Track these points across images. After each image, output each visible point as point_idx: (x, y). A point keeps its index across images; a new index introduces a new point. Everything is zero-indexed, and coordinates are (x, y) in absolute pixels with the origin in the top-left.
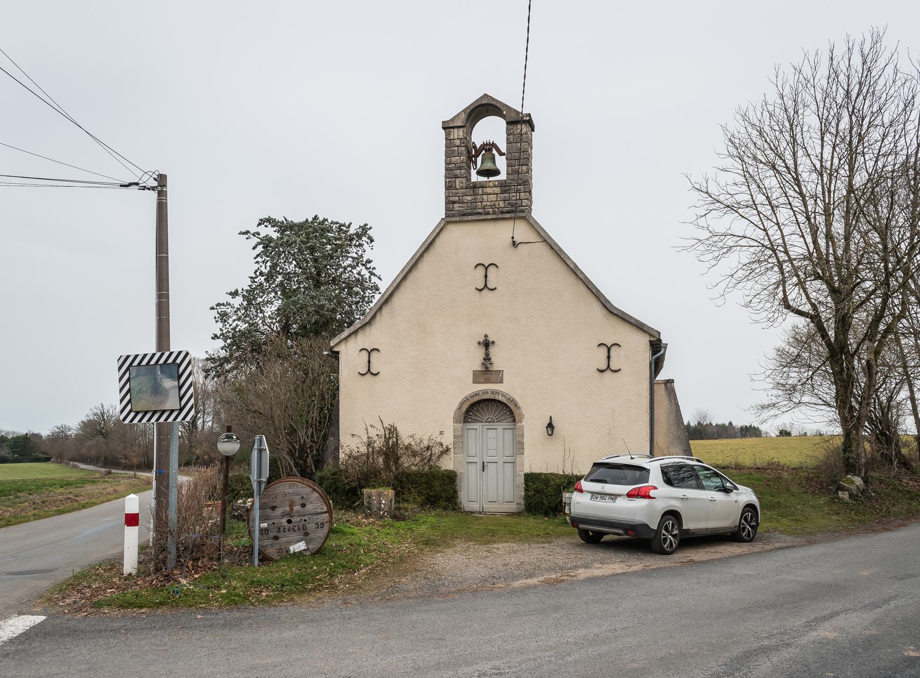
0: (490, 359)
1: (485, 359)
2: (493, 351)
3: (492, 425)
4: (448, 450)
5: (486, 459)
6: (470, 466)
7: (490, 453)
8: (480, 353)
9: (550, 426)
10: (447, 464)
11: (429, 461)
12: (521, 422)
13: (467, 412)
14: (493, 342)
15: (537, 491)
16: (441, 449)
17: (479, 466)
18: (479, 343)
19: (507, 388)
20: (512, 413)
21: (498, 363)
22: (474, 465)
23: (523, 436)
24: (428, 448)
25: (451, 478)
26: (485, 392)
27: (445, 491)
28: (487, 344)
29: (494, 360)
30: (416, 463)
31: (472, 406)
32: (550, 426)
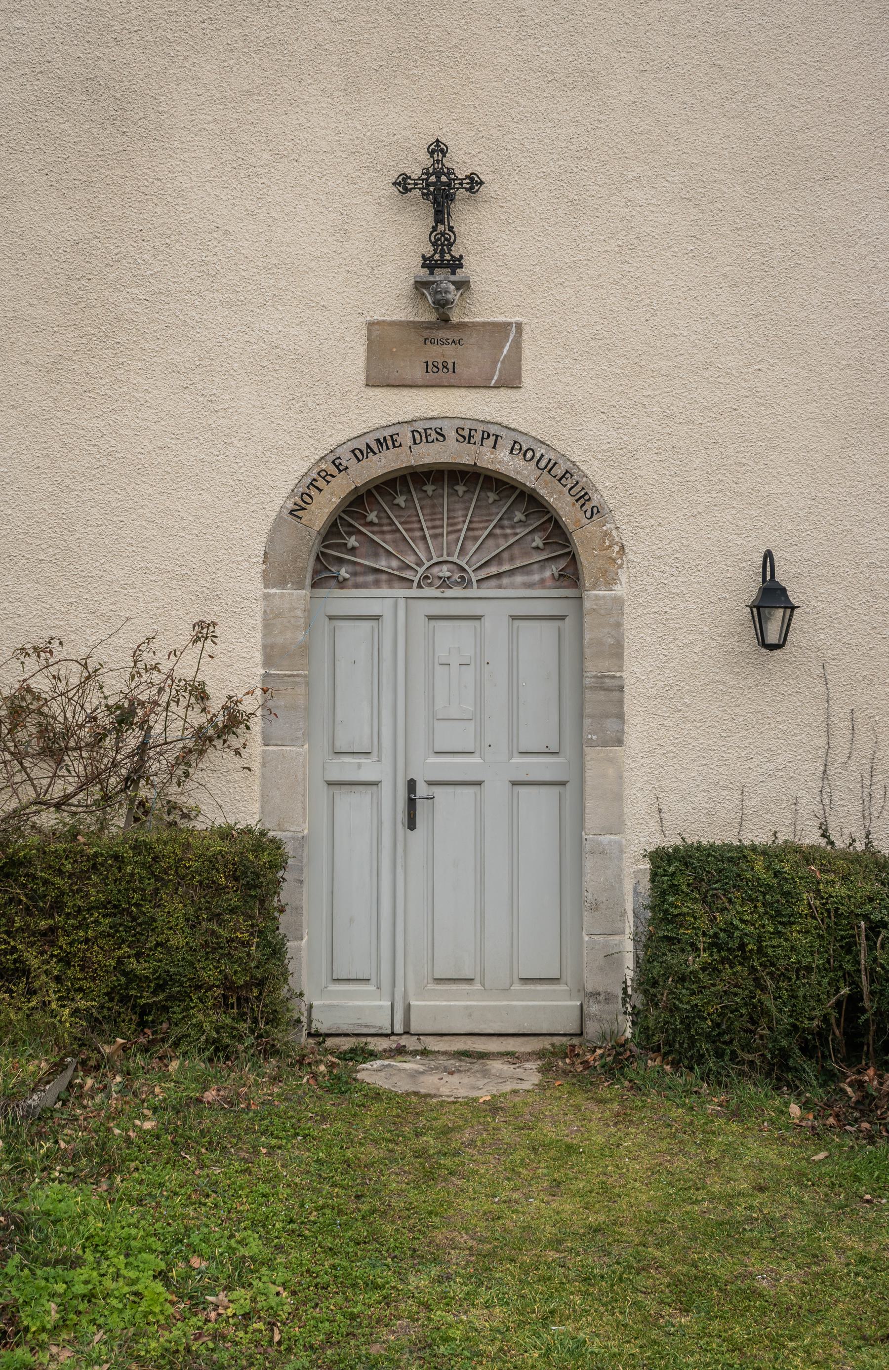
0: (456, 264)
1: (429, 264)
2: (471, 224)
3: (455, 601)
4: (233, 721)
5: (426, 767)
6: (344, 800)
7: (452, 736)
8: (406, 236)
9: (771, 598)
10: (227, 797)
11: (131, 781)
12: (611, 581)
13: (334, 531)
14: (474, 183)
15: (728, 949)
16: (197, 719)
17: (392, 800)
18: (403, 184)
19: (547, 408)
20: (556, 536)
21: (494, 289)
22: (363, 799)
23: (617, 652)
24: (125, 716)
25: (250, 873)
26: (428, 432)
27: (214, 948)
28: (440, 190)
29: (474, 268)
30: (57, 792)
31: (360, 502)
32: (771, 598)
